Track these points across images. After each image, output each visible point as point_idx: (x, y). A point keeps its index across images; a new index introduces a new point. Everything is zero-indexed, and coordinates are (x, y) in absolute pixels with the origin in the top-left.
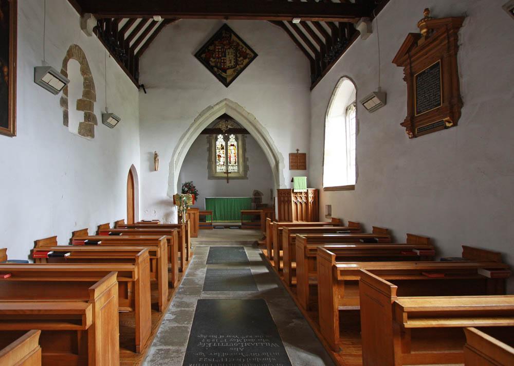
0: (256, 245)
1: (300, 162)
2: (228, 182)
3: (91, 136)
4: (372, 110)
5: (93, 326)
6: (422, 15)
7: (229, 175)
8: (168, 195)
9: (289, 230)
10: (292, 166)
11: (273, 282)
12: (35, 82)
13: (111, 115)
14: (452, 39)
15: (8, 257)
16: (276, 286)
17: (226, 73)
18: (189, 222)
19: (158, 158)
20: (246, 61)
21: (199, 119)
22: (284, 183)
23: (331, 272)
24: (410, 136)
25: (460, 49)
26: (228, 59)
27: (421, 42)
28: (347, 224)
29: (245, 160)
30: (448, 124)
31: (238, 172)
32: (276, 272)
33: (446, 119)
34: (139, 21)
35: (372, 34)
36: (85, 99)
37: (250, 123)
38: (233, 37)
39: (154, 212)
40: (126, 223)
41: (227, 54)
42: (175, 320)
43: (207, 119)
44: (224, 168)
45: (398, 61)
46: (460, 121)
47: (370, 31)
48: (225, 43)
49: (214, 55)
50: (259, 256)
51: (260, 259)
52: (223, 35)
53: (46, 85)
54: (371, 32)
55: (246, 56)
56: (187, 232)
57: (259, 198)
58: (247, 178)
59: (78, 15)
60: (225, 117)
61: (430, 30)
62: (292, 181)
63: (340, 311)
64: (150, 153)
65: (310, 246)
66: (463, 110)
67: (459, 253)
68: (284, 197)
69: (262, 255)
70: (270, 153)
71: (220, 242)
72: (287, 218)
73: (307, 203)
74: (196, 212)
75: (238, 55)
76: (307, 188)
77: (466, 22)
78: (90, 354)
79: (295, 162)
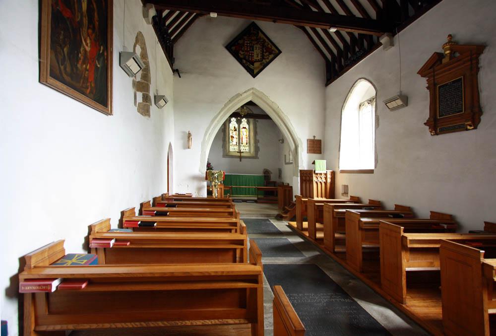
0: (279, 218)
2: (241, 161)
3: (148, 115)
4: (393, 109)
6: (446, 40)
7: (242, 154)
8: (200, 171)
9: (332, 206)
10: (310, 150)
12: (120, 65)
13: (162, 97)
14: (474, 62)
17: (253, 65)
19: (192, 137)
20: (271, 56)
24: (432, 134)
25: (480, 70)
26: (255, 53)
27: (445, 61)
29: (256, 142)
30: (469, 127)
31: (250, 152)
33: (468, 123)
34: (178, 12)
35: (393, 47)
36: (143, 81)
38: (260, 34)
39: (187, 186)
41: (255, 48)
44: (236, 148)
45: (422, 73)
46: (480, 126)
47: (392, 44)
48: (253, 38)
49: (243, 49)
51: (288, 230)
52: (252, 31)
53: (127, 69)
54: (393, 45)
55: (270, 53)
57: (268, 176)
59: (142, 4)
60: (251, 103)
61: (453, 52)
62: (314, 163)
63: (408, 272)
64: (184, 132)
66: (482, 117)
67: (481, 227)
68: (306, 177)
70: (290, 138)
71: (247, 214)
72: (308, 195)
73: (326, 183)
75: (265, 50)
76: (327, 169)
77: (486, 51)
79: (312, 147)
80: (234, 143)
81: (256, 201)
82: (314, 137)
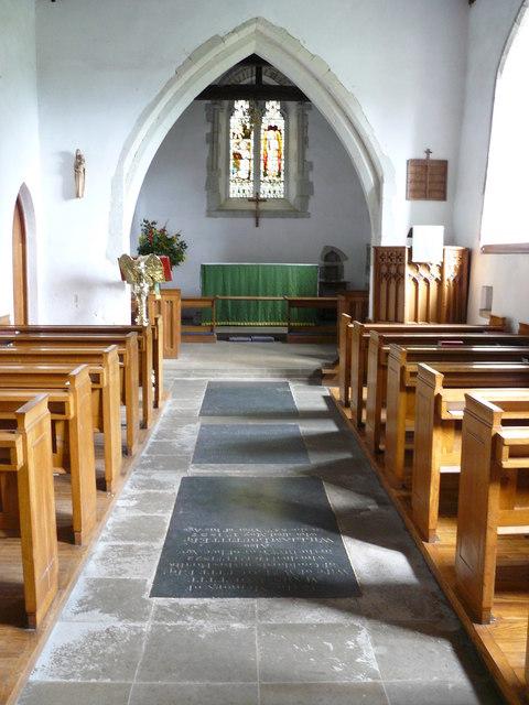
0: (315, 378)
1: (431, 180)
5: (26, 467)
7: (262, 206)
11: (340, 448)
15: (383, 238)
16: (348, 455)
18: (160, 322)
19: (86, 165)
21: (187, 69)
22: (391, 235)
23: (433, 406)
28: (516, 327)
29: (305, 167)
32: (352, 427)
37: (314, 76)
40: (12, 323)
42: (137, 507)
43: (209, 66)
50: (322, 399)
51: (323, 406)
56: (155, 342)
57: (336, 267)
58: (308, 215)
60: (254, 61)
64: (65, 154)
65: (411, 367)
69: (328, 400)
73: (440, 283)
74: (174, 298)
76: (445, 244)
78: (22, 511)
79: (421, 181)
80: (243, 174)
81: (279, 338)
82: (428, 152)
